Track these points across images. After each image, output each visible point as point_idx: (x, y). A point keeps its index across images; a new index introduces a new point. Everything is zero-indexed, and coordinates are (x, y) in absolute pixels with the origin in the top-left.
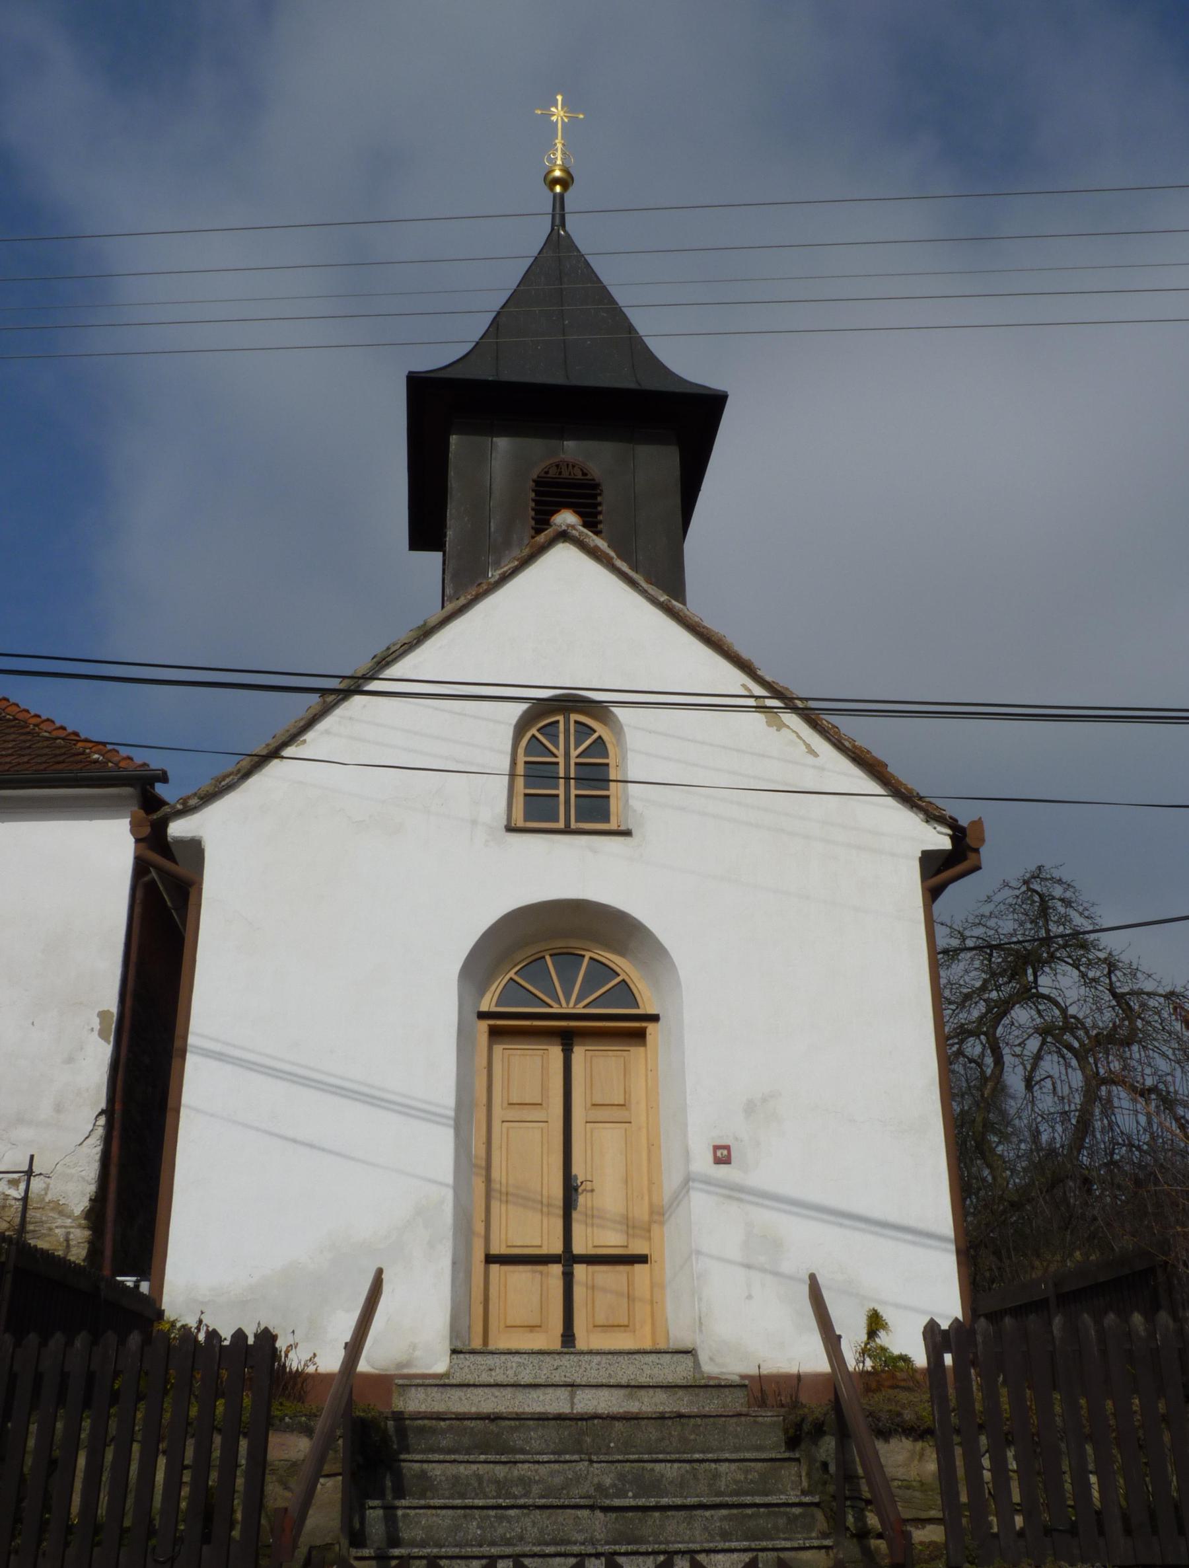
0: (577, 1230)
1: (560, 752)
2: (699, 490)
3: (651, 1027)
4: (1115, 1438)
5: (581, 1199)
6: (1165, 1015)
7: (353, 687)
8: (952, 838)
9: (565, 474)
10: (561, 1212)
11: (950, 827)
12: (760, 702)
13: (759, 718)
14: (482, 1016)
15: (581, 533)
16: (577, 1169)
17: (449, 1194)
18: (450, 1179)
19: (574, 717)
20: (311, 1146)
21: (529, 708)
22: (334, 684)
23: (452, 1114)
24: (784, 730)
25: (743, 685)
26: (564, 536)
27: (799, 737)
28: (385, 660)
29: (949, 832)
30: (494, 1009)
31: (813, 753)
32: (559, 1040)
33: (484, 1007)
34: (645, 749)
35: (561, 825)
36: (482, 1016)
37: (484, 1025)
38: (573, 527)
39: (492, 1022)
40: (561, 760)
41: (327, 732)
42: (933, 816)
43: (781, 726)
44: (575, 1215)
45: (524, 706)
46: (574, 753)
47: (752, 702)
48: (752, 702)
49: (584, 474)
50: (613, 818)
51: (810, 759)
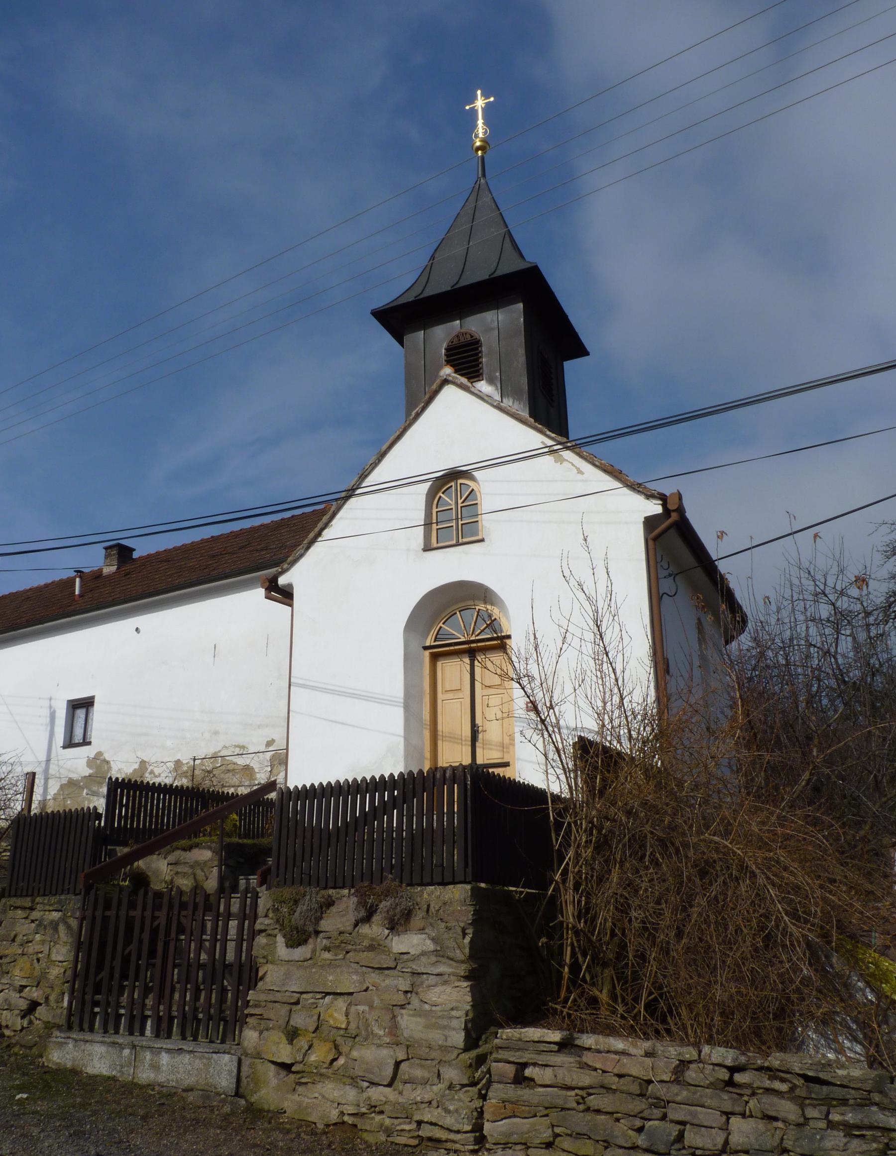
0: (479, 751)
1: (453, 503)
2: (566, 317)
3: (508, 641)
4: (127, 980)
5: (480, 736)
6: (808, 603)
7: (350, 493)
8: (662, 505)
9: (462, 340)
10: (470, 743)
11: (661, 499)
12: (552, 449)
13: (549, 459)
14: (426, 648)
15: (453, 377)
16: (478, 721)
17: (402, 740)
18: (402, 733)
19: (460, 481)
20: (343, 723)
21: (431, 486)
22: (343, 494)
23: (402, 701)
24: (565, 463)
25: (542, 442)
26: (446, 382)
27: (573, 465)
28: (364, 476)
29: (660, 502)
30: (433, 644)
31: (580, 472)
32: (467, 655)
33: (428, 644)
34: (490, 489)
35: (454, 542)
36: (426, 648)
37: (427, 653)
38: (449, 375)
39: (431, 651)
40: (453, 507)
41: (341, 518)
42: (649, 496)
43: (561, 460)
44: (477, 744)
45: (427, 485)
46: (460, 501)
47: (546, 450)
48: (546, 450)
49: (472, 337)
50: (480, 533)
51: (580, 477)
